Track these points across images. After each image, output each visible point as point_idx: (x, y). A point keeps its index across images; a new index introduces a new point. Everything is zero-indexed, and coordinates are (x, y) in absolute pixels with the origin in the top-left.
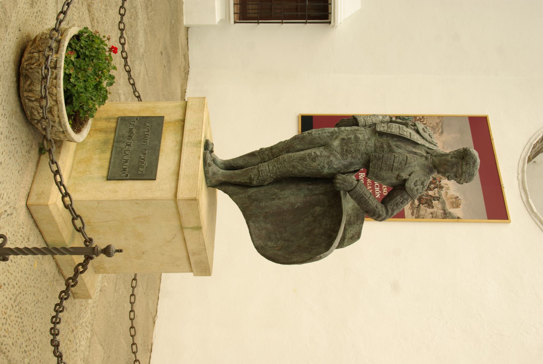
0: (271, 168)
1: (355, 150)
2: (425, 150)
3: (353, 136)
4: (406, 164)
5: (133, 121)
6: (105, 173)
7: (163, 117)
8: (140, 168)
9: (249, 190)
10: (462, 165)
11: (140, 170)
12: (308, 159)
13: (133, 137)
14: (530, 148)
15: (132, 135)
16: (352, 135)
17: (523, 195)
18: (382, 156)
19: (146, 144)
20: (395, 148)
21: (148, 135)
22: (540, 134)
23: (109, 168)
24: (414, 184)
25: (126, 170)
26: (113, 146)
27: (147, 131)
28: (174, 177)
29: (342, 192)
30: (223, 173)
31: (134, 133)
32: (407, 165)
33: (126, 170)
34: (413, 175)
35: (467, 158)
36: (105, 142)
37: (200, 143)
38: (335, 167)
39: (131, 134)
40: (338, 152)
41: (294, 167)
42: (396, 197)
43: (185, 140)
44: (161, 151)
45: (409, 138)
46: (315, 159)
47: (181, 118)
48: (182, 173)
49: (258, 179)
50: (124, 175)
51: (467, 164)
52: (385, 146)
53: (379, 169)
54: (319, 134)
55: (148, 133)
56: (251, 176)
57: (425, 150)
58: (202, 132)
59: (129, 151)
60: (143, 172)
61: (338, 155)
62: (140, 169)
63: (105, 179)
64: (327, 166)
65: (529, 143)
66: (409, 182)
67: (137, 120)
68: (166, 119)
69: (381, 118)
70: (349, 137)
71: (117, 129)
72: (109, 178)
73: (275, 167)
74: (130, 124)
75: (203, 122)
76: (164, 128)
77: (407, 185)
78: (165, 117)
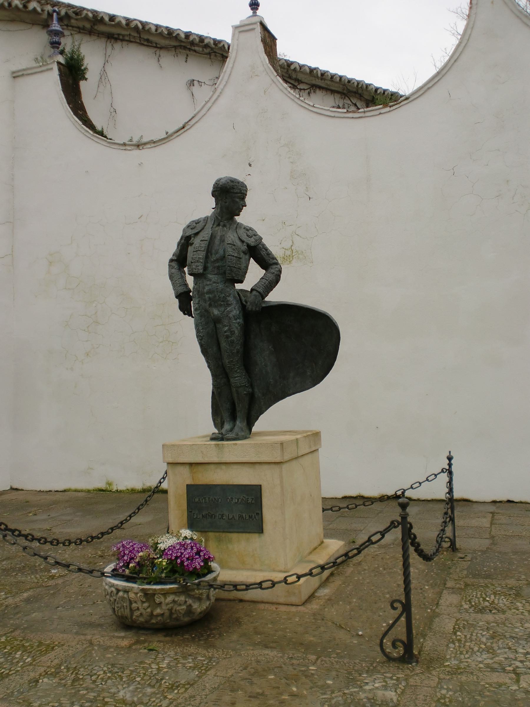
0: (238, 375)
1: (222, 293)
2: (216, 227)
3: (207, 296)
4: (234, 245)
5: (194, 516)
6: (256, 535)
7: (187, 485)
8: (249, 502)
9: (256, 396)
10: (234, 193)
11: (250, 501)
12: (232, 338)
13: (212, 513)
14: (96, 137)
15: (210, 514)
16: (205, 296)
17: (149, 146)
18: (229, 268)
19: (220, 500)
20: (218, 256)
21: (209, 498)
22: (82, 127)
23: (249, 532)
24: (251, 238)
25: (251, 516)
26: (223, 532)
27: (205, 500)
28: (257, 466)
29: (264, 305)
30: (240, 422)
31: (207, 513)
32: (235, 244)
33: (251, 516)
34: (243, 239)
35: (228, 187)
36: (219, 540)
37: (218, 445)
38: (238, 312)
39: (209, 515)
40: (225, 310)
41: (238, 352)
42: (262, 255)
43: (215, 460)
44: (228, 483)
45: (207, 242)
46: (232, 332)
47: (187, 467)
48: (254, 460)
49: (247, 387)
50: (257, 517)
51: (233, 188)
52: (217, 265)
53: (239, 270)
54: (203, 329)
55: (207, 499)
56: (244, 394)
57: (216, 227)
58: (205, 444)
59: (228, 515)
60: (253, 499)
61: (228, 309)
62: (250, 501)
63: (261, 535)
64: (238, 320)
65: (92, 138)
66: (249, 242)
67: (191, 512)
68: (189, 482)
69: (173, 271)
70: (207, 299)
71: (203, 530)
72: (260, 530)
73: (237, 370)
74: (197, 518)
75: (193, 445)
76: (200, 483)
77: (252, 244)
78: (187, 484)
